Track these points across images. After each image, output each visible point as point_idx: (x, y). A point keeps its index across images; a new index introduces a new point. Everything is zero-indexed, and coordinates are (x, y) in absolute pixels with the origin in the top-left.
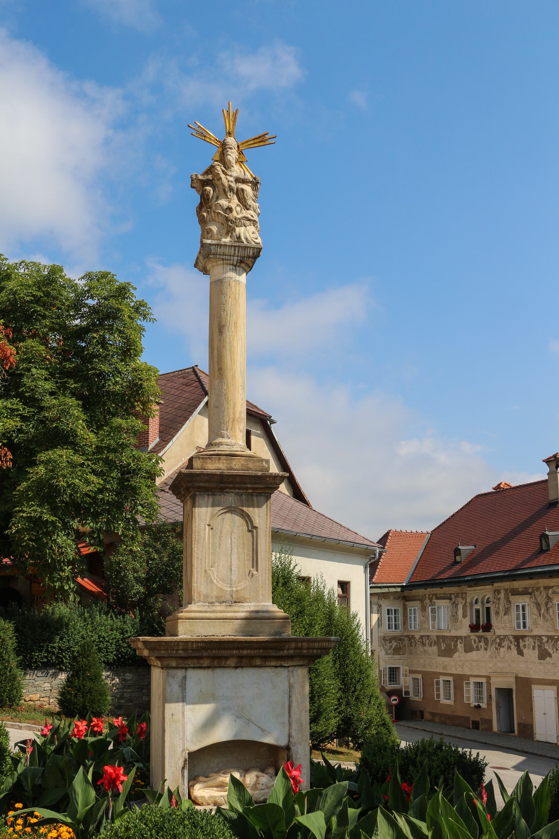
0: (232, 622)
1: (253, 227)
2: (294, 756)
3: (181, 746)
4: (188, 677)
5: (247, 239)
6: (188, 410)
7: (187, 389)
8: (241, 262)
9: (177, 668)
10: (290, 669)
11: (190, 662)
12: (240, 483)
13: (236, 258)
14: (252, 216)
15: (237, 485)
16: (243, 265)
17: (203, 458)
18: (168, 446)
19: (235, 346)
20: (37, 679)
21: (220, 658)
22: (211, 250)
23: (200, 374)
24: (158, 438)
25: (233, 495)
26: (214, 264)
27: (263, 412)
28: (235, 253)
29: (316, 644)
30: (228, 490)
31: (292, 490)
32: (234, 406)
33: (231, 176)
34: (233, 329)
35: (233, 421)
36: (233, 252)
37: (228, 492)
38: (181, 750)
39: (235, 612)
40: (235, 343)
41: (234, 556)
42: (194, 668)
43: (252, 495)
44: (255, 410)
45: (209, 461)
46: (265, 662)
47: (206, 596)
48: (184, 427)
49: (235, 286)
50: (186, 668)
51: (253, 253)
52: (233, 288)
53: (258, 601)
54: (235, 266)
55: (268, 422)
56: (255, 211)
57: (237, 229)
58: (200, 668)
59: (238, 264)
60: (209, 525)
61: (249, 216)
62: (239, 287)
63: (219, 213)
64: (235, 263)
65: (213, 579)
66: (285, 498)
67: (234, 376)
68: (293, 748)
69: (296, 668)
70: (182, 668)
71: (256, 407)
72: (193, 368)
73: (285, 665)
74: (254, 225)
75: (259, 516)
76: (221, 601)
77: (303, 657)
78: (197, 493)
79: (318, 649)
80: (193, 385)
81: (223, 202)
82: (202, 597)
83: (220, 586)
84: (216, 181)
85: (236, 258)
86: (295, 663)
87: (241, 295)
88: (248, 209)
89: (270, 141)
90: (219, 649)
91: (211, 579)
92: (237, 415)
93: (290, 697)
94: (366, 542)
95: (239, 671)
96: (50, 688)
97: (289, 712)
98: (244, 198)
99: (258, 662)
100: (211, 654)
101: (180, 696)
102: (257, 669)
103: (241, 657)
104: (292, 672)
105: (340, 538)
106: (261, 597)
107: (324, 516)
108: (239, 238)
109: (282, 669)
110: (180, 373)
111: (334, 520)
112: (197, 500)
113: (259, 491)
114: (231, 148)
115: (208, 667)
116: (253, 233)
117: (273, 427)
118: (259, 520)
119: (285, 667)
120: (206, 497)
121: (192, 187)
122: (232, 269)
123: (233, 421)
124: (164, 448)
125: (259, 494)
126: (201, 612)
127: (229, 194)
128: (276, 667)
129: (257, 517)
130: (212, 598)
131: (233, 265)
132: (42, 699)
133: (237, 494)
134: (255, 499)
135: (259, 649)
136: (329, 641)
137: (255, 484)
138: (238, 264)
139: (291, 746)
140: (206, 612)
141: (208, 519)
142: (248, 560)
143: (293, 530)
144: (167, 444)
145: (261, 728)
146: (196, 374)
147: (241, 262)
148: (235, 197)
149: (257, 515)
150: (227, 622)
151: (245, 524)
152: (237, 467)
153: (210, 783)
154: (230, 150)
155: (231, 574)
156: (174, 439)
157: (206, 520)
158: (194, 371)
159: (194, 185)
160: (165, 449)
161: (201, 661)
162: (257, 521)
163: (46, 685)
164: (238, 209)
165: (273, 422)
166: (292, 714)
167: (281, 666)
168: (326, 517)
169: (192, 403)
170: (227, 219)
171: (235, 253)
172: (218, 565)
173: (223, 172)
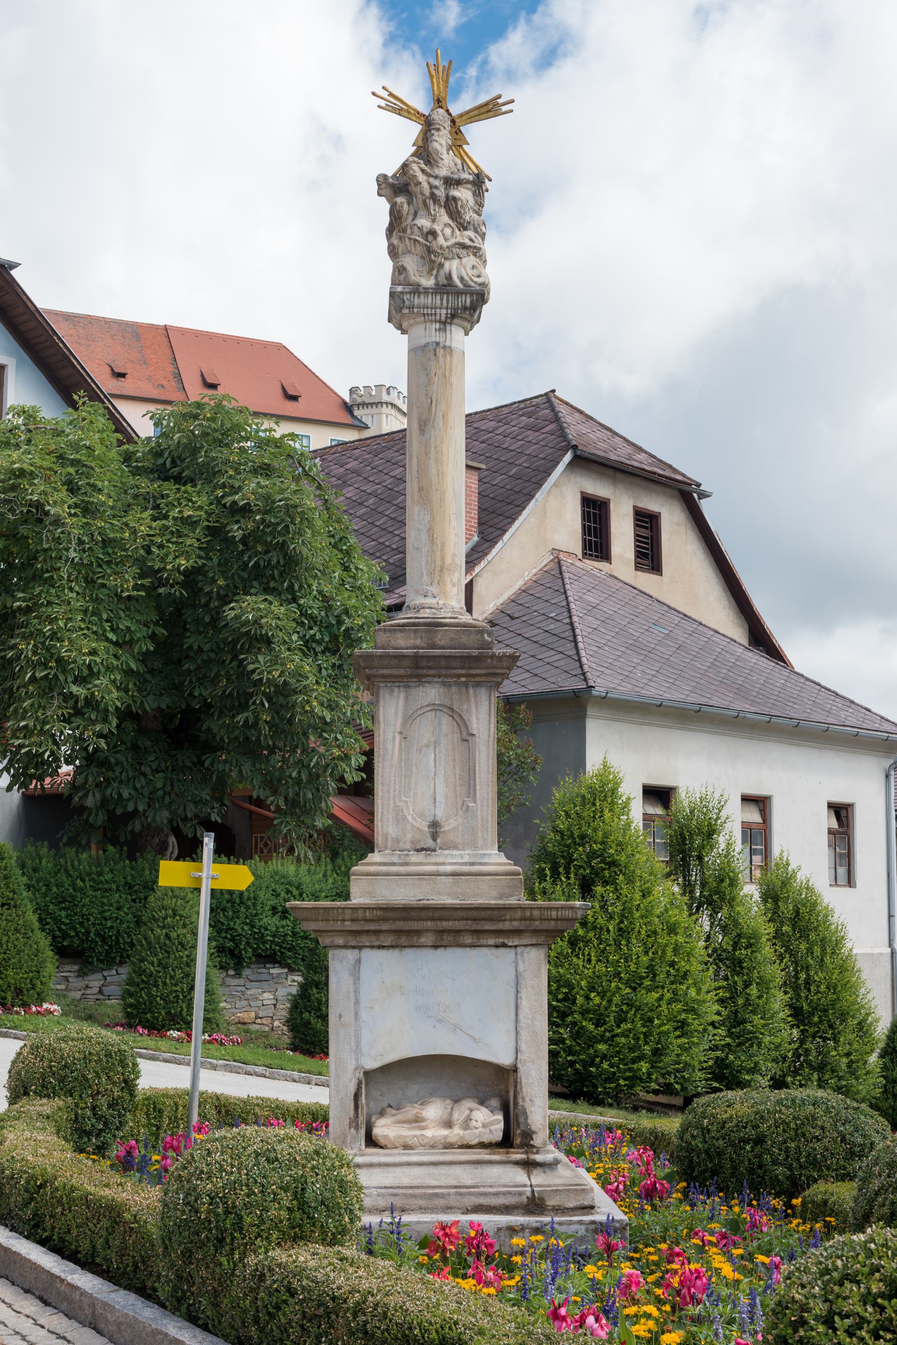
1: (472, 257)
2: (524, 1080)
3: (354, 1062)
5: (462, 279)
6: (534, 480)
7: (532, 436)
9: (345, 947)
10: (519, 950)
11: (366, 940)
12: (447, 668)
14: (471, 240)
15: (443, 672)
16: (456, 321)
17: (390, 631)
18: (494, 551)
20: (248, 985)
21: (409, 933)
22: (404, 302)
23: (562, 409)
24: (476, 535)
25: (437, 686)
26: (412, 321)
27: (683, 475)
29: (554, 913)
30: (427, 679)
31: (746, 626)
33: (436, 177)
34: (441, 424)
36: (438, 302)
37: (429, 682)
38: (353, 1067)
39: (437, 864)
41: (440, 780)
42: (372, 947)
43: (466, 685)
44: (667, 473)
45: (399, 635)
46: (478, 939)
47: (397, 841)
48: (525, 513)
49: (444, 356)
50: (360, 948)
51: (472, 302)
52: (441, 360)
53: (476, 848)
54: (445, 323)
55: (695, 495)
56: (477, 232)
57: (447, 265)
58: (380, 947)
60: (401, 733)
61: (467, 242)
62: (451, 355)
63: (416, 240)
64: (443, 319)
66: (724, 643)
68: (522, 1069)
69: (528, 949)
70: (354, 947)
71: (670, 467)
72: (546, 394)
74: (475, 255)
75: (478, 719)
76: (419, 847)
77: (536, 932)
78: (382, 685)
79: (557, 919)
80: (544, 431)
81: (423, 222)
82: (390, 841)
84: (412, 188)
85: (444, 311)
86: (525, 942)
87: (454, 370)
88: (465, 229)
89: (504, 108)
90: (405, 919)
92: (448, 561)
93: (517, 992)
94: (887, 727)
95: (440, 951)
96: (273, 1002)
97: (517, 1015)
98: (458, 212)
99: (468, 940)
100: (393, 928)
101: (352, 989)
102: (468, 949)
103: (440, 932)
104: (522, 955)
105: (830, 720)
106: (480, 842)
107: (802, 676)
108: (449, 277)
109: (507, 950)
110: (522, 406)
111: (823, 684)
112: (381, 695)
113: (478, 679)
114: (438, 130)
115: (392, 947)
116: (473, 267)
117: (705, 505)
120: (396, 690)
121: (379, 195)
124: (486, 554)
126: (384, 864)
127: (432, 208)
128: (497, 946)
130: (405, 843)
131: (440, 321)
132: (259, 1021)
133: (444, 684)
134: (471, 691)
135: (467, 919)
136: (572, 908)
137: (470, 668)
139: (519, 1065)
140: (393, 864)
141: (399, 724)
142: (461, 785)
143: (732, 706)
144: (493, 546)
146: (553, 409)
147: (453, 316)
148: (443, 211)
151: (456, 729)
152: (443, 643)
153: (399, 1117)
154: (436, 133)
155: (435, 807)
156: (506, 537)
157: (395, 725)
158: (549, 401)
159: (382, 192)
160: (489, 557)
161: (382, 938)
162: (475, 725)
163: (266, 995)
164: (448, 231)
165: (704, 495)
166: (521, 1017)
167: (504, 945)
168: (807, 679)
169: (541, 465)
170: (429, 250)
172: (415, 794)
173: (423, 171)
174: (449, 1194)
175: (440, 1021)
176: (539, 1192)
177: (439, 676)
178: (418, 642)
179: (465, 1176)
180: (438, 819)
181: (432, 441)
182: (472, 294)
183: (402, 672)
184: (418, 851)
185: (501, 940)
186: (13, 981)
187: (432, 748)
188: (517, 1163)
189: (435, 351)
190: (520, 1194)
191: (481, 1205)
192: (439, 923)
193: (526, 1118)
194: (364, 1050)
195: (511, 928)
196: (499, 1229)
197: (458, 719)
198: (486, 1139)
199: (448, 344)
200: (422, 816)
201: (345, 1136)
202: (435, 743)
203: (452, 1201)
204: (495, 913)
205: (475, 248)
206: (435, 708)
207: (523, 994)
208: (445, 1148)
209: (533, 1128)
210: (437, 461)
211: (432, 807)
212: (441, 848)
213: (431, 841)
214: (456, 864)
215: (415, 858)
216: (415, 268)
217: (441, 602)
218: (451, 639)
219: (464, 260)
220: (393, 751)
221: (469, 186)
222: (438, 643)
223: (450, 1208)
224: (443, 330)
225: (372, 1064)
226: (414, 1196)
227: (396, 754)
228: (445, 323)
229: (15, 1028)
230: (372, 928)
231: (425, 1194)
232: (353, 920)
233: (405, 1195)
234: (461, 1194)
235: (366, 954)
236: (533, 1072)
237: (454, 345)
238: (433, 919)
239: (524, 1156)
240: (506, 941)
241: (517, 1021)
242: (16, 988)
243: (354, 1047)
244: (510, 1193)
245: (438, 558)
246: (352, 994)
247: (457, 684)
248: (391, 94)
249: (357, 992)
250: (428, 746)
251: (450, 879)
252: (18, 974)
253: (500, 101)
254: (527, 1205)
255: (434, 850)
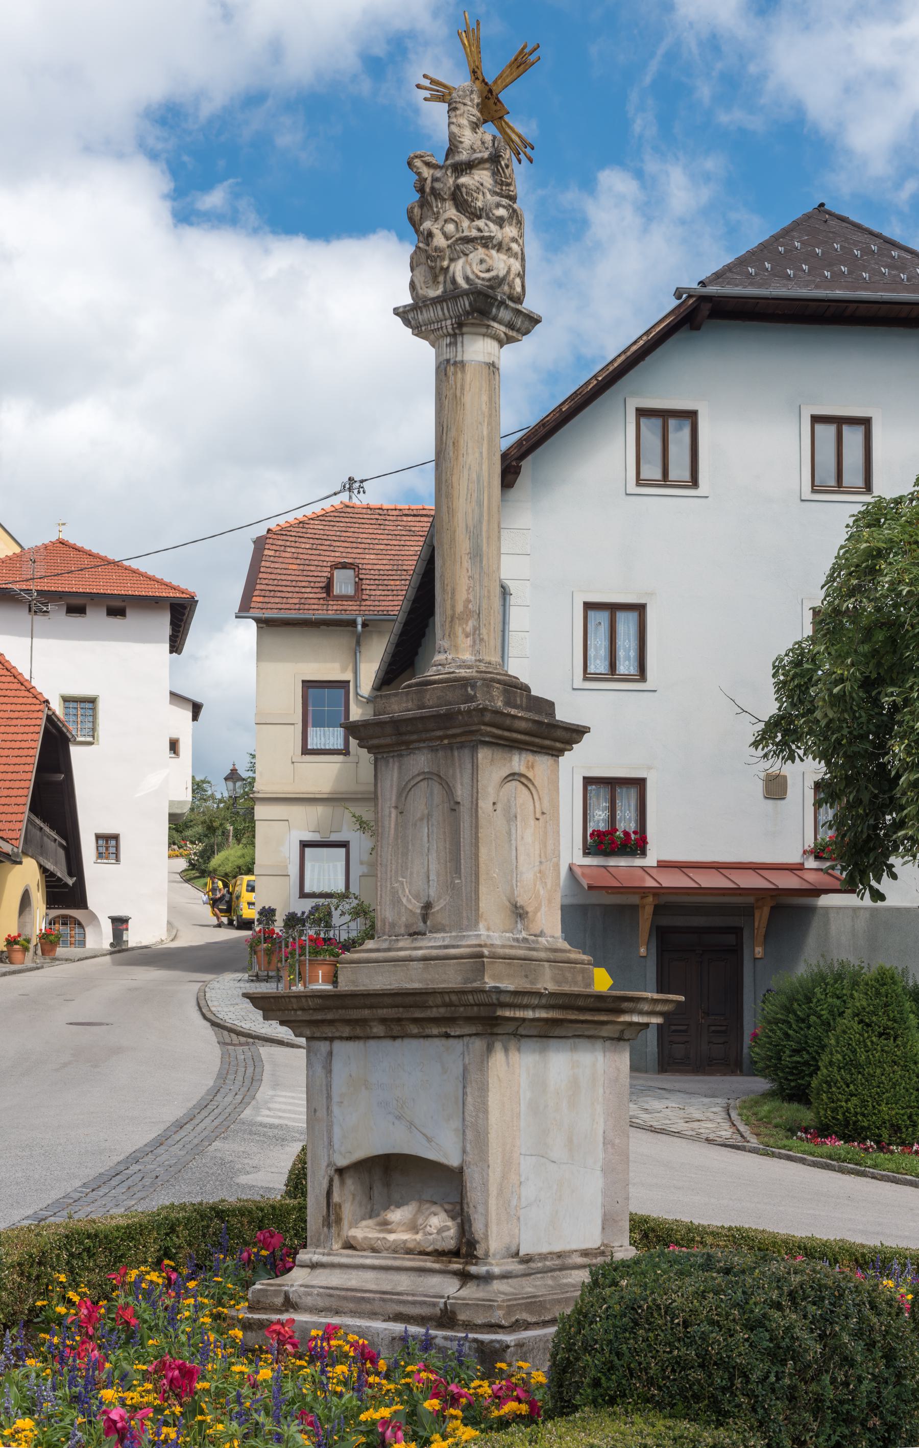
0: (405, 965)
2: (468, 1184)
3: (326, 1158)
4: (334, 1052)
5: (467, 279)
8: (460, 325)
13: (449, 322)
14: (479, 230)
15: (424, 736)
16: (465, 329)
19: (455, 485)
25: (425, 751)
28: (444, 314)
30: (417, 745)
31: (423, 640)
32: (453, 593)
34: (451, 453)
35: (452, 621)
36: (440, 313)
37: (418, 748)
38: (325, 1164)
40: (455, 479)
41: (433, 856)
47: (393, 925)
49: (455, 374)
50: (331, 1039)
51: (470, 304)
52: (452, 378)
59: (457, 331)
60: (396, 807)
64: (450, 331)
65: (401, 896)
67: (453, 540)
68: (467, 1171)
69: (473, 1039)
70: (326, 1039)
73: (586, 1033)
74: (485, 246)
75: (462, 785)
76: (411, 931)
82: (387, 927)
83: (410, 907)
85: (449, 322)
87: (467, 387)
89: (532, 58)
91: (399, 897)
92: (460, 608)
106: (465, 922)
116: (482, 261)
118: (462, 790)
119: (459, 1037)
120: (391, 760)
122: (450, 343)
123: (452, 621)
125: (462, 746)
129: (459, 786)
131: (449, 335)
134: (456, 753)
135: (397, 1007)
138: (457, 331)
141: (394, 798)
145: (426, 1137)
147: (460, 325)
148: (449, 205)
149: (459, 781)
150: (399, 966)
155: (429, 886)
157: (391, 800)
162: (459, 792)
171: (444, 314)
172: (412, 873)
174: (374, 1299)
175: (399, 1118)
176: (451, 1304)
177: (424, 741)
178: (410, 705)
179: (403, 1283)
180: (431, 899)
181: (444, 474)
182: (467, 295)
183: (388, 740)
184: (410, 935)
185: (444, 1030)
186: (887, 1117)
187: (425, 821)
188: (455, 1273)
189: (446, 371)
190: (434, 1305)
191: (401, 1314)
192: (375, 1011)
193: (470, 1227)
194: (336, 1147)
195: (438, 1015)
196: (394, 1339)
197: (446, 787)
198: (440, 1246)
199: (459, 358)
200: (417, 897)
201: (320, 1234)
202: (428, 815)
203: (377, 1307)
204: (418, 998)
205: (482, 238)
206: (428, 776)
207: (469, 1090)
208: (407, 1253)
209: (477, 1237)
210: (447, 497)
211: (426, 887)
212: (431, 932)
213: (422, 924)
214: (432, 947)
215: (404, 942)
216: (422, 279)
217: (450, 657)
218: (439, 698)
219: (471, 256)
220: (390, 827)
221: (487, 165)
222: (428, 703)
223: (375, 1314)
224: (453, 344)
225: (342, 1162)
226: (345, 1298)
227: (392, 831)
228: (454, 335)
229: (875, 1166)
230: (319, 1017)
231: (355, 1297)
232: (303, 1009)
233: (339, 1296)
234: (383, 1300)
235: (338, 1046)
236: (476, 1176)
237: (466, 358)
238: (371, 1007)
239: (459, 1266)
240: (448, 1030)
241: (464, 1119)
242: (892, 1125)
243: (326, 1144)
244: (424, 1303)
245: (448, 607)
246: (324, 1088)
247: (444, 747)
248: (433, 82)
249: (329, 1086)
250: (421, 819)
251: (421, 965)
252: (893, 1109)
253: (527, 50)
254: (440, 1318)
255: (425, 934)
